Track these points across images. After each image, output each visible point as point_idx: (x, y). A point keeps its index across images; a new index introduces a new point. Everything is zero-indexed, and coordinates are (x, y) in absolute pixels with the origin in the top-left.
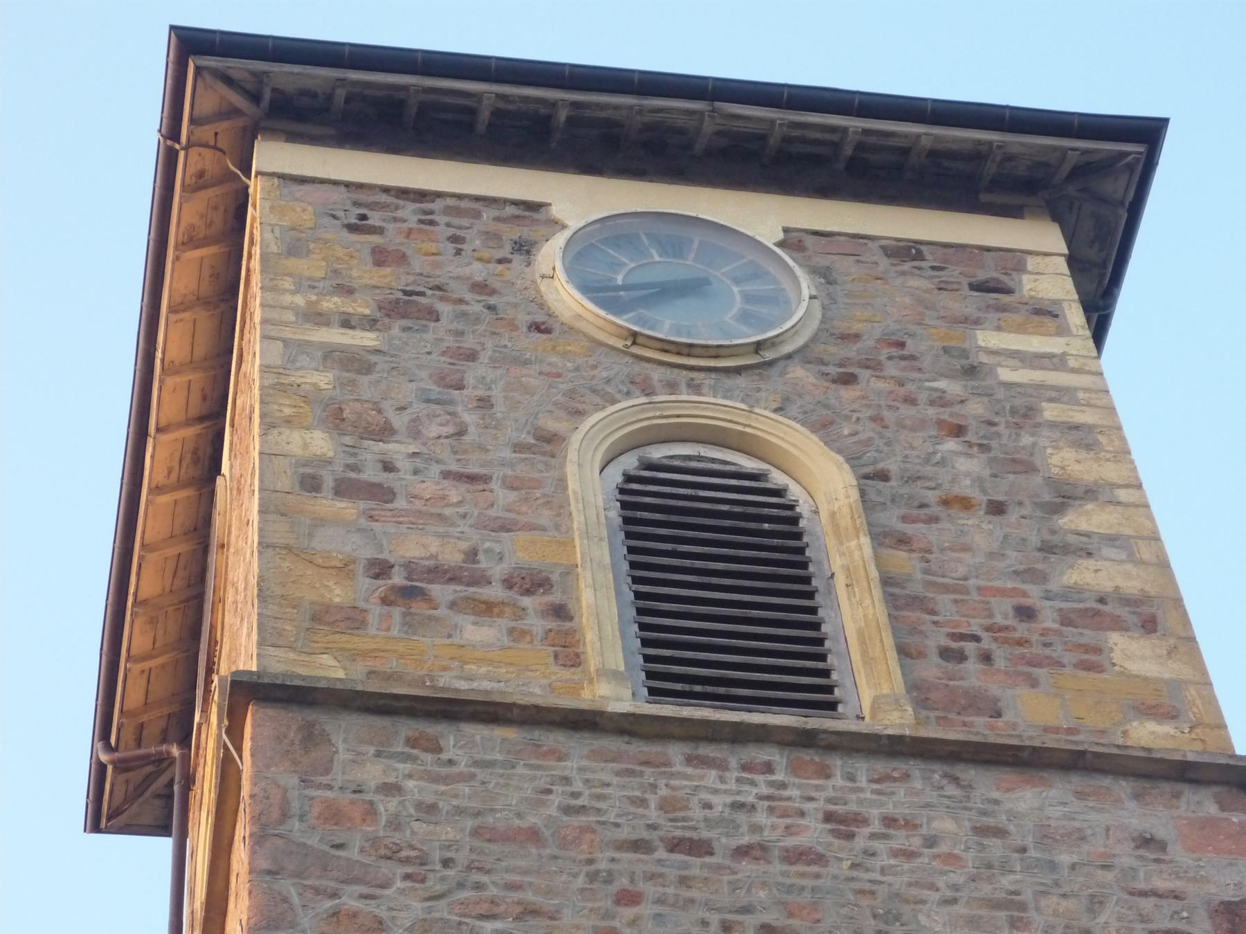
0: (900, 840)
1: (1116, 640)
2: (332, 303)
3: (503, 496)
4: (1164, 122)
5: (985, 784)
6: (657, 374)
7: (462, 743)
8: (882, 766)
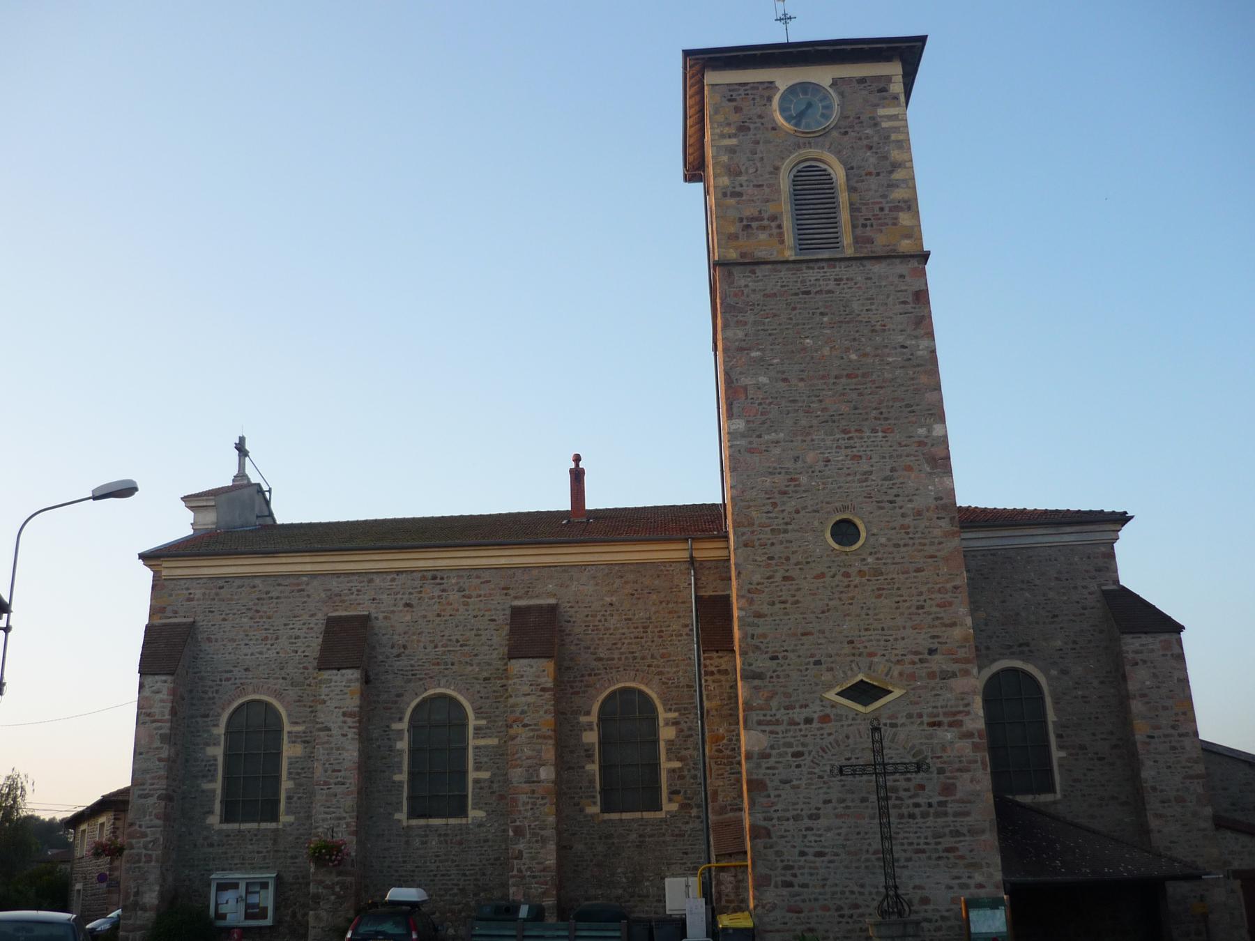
0: (851, 284)
1: (901, 214)
2: (726, 130)
3: (767, 190)
4: (922, 40)
5: (868, 264)
6: (801, 141)
7: (761, 271)
8: (847, 263)
